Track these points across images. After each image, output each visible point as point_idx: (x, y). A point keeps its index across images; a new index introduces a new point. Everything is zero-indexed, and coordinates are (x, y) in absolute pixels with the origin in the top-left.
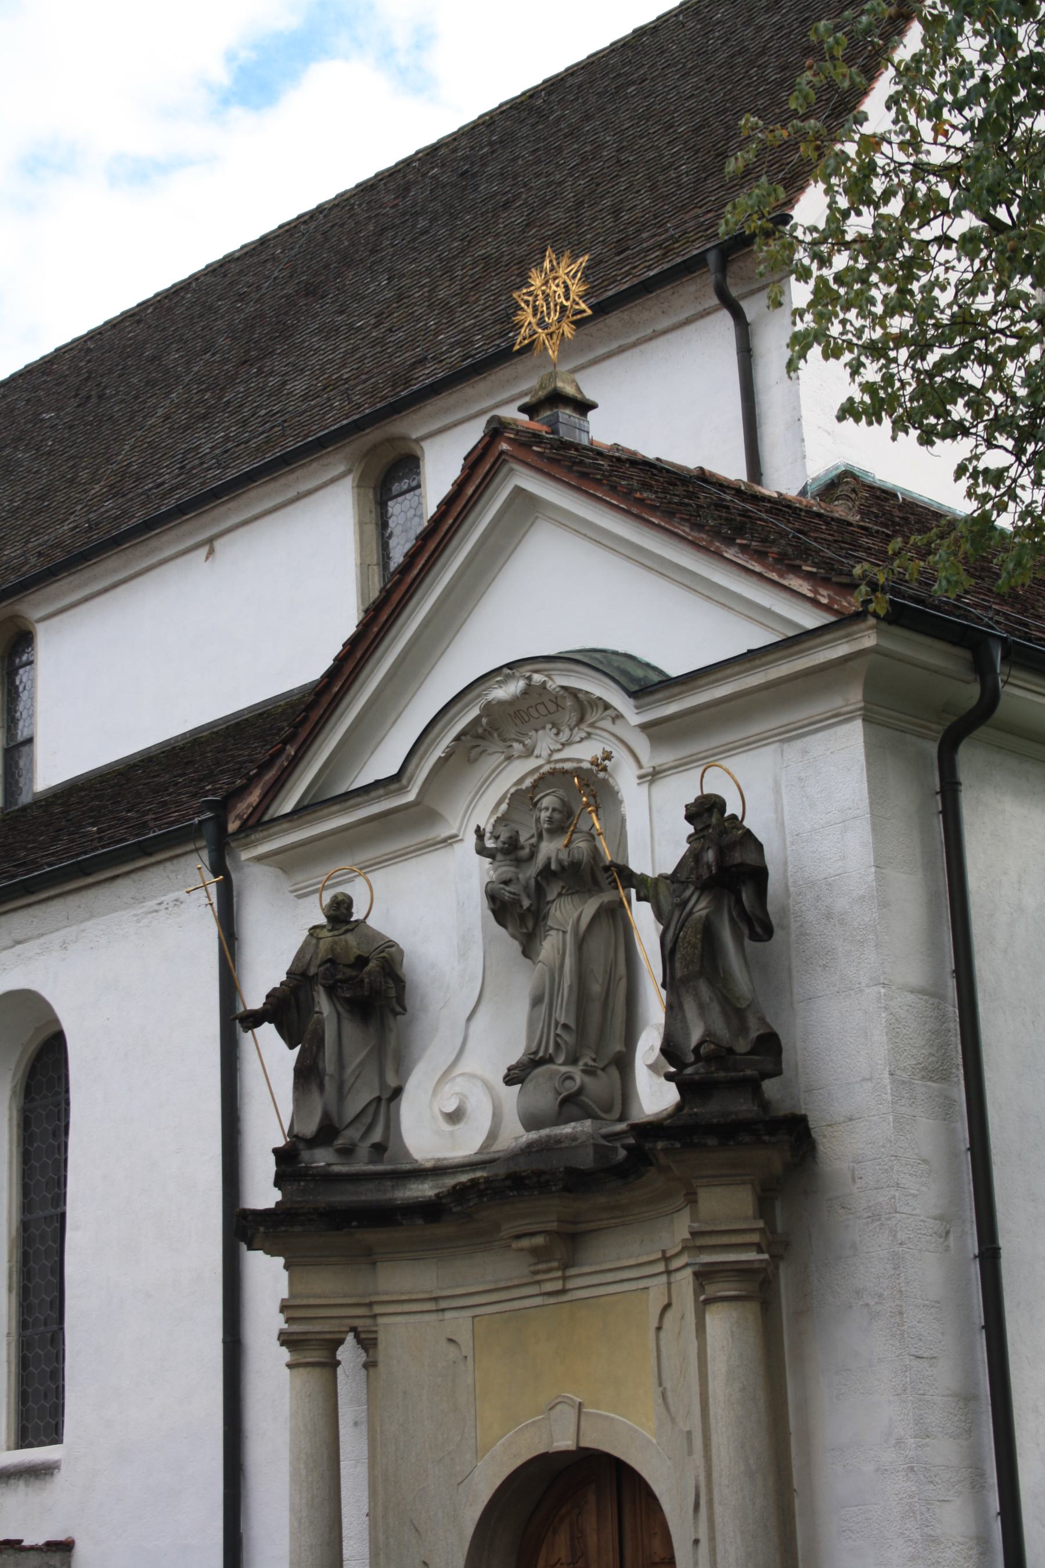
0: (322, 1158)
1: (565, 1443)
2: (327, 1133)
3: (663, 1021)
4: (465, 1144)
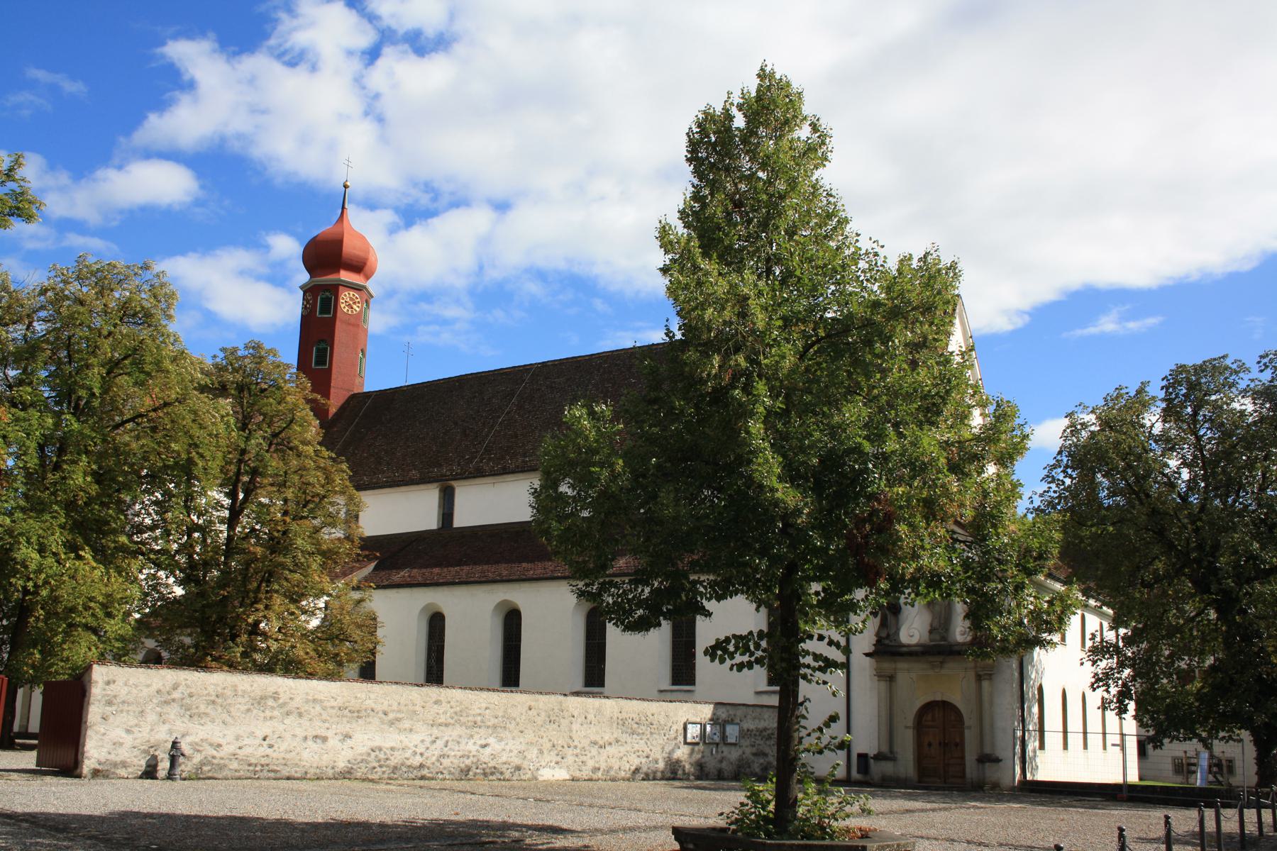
0: (887, 642)
1: (939, 698)
2: (888, 636)
3: (366, 389)
4: (914, 641)
